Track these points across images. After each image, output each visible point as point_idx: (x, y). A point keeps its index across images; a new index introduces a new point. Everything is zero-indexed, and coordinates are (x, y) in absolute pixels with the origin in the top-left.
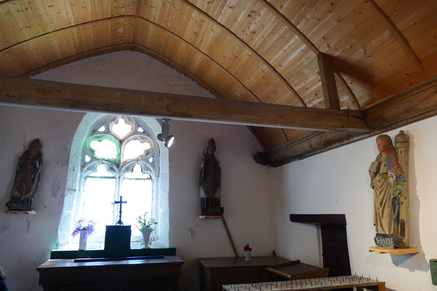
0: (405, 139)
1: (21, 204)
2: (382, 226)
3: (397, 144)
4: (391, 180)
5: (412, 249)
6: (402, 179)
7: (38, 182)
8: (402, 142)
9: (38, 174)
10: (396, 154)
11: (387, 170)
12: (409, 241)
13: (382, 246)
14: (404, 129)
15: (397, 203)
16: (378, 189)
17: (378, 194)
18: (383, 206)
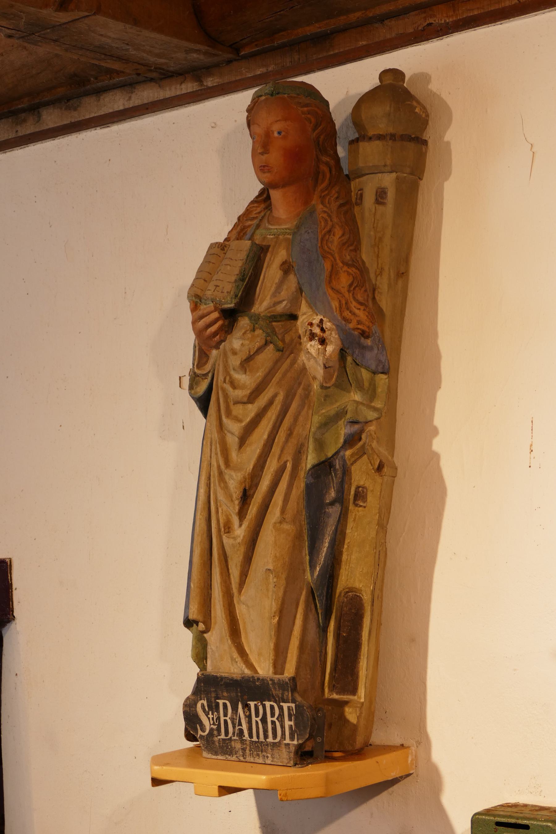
0: (405, 122)
2: (235, 631)
3: (365, 148)
4: (314, 357)
5: (385, 759)
6: (370, 357)
8: (393, 137)
10: (348, 206)
11: (295, 301)
12: (370, 713)
13: (225, 749)
14: (407, 59)
15: (332, 494)
16: (237, 410)
17: (232, 441)
18: (253, 510)
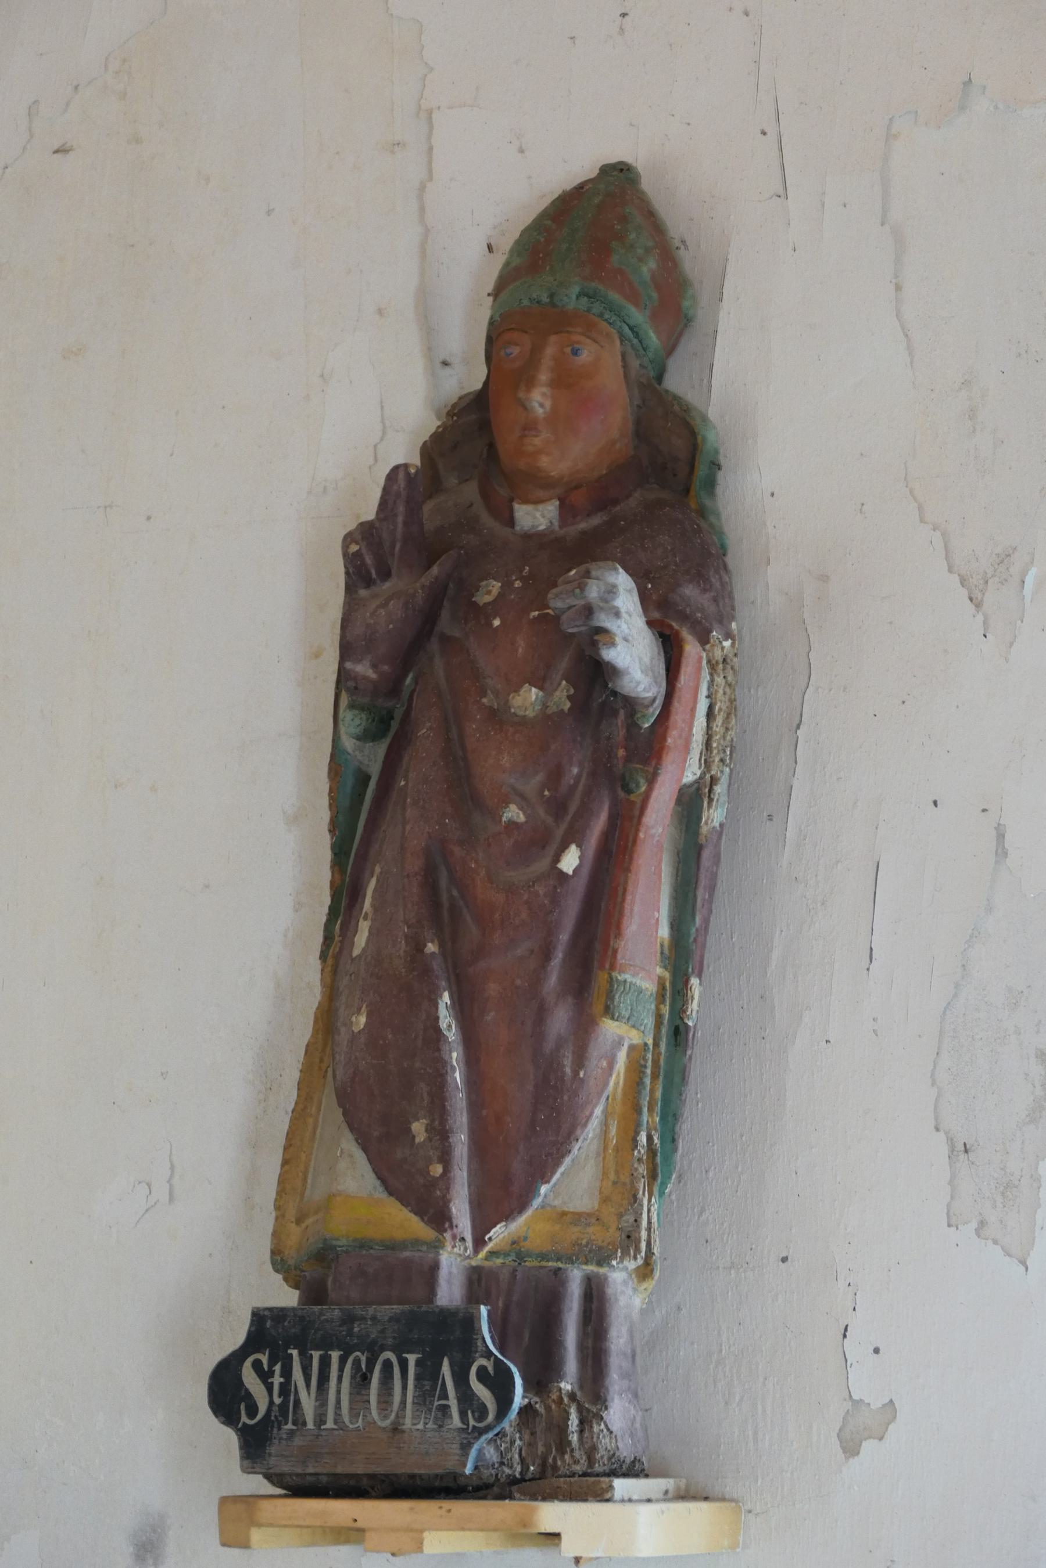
1: (429, 1373)
7: (682, 958)
9: (658, 821)
